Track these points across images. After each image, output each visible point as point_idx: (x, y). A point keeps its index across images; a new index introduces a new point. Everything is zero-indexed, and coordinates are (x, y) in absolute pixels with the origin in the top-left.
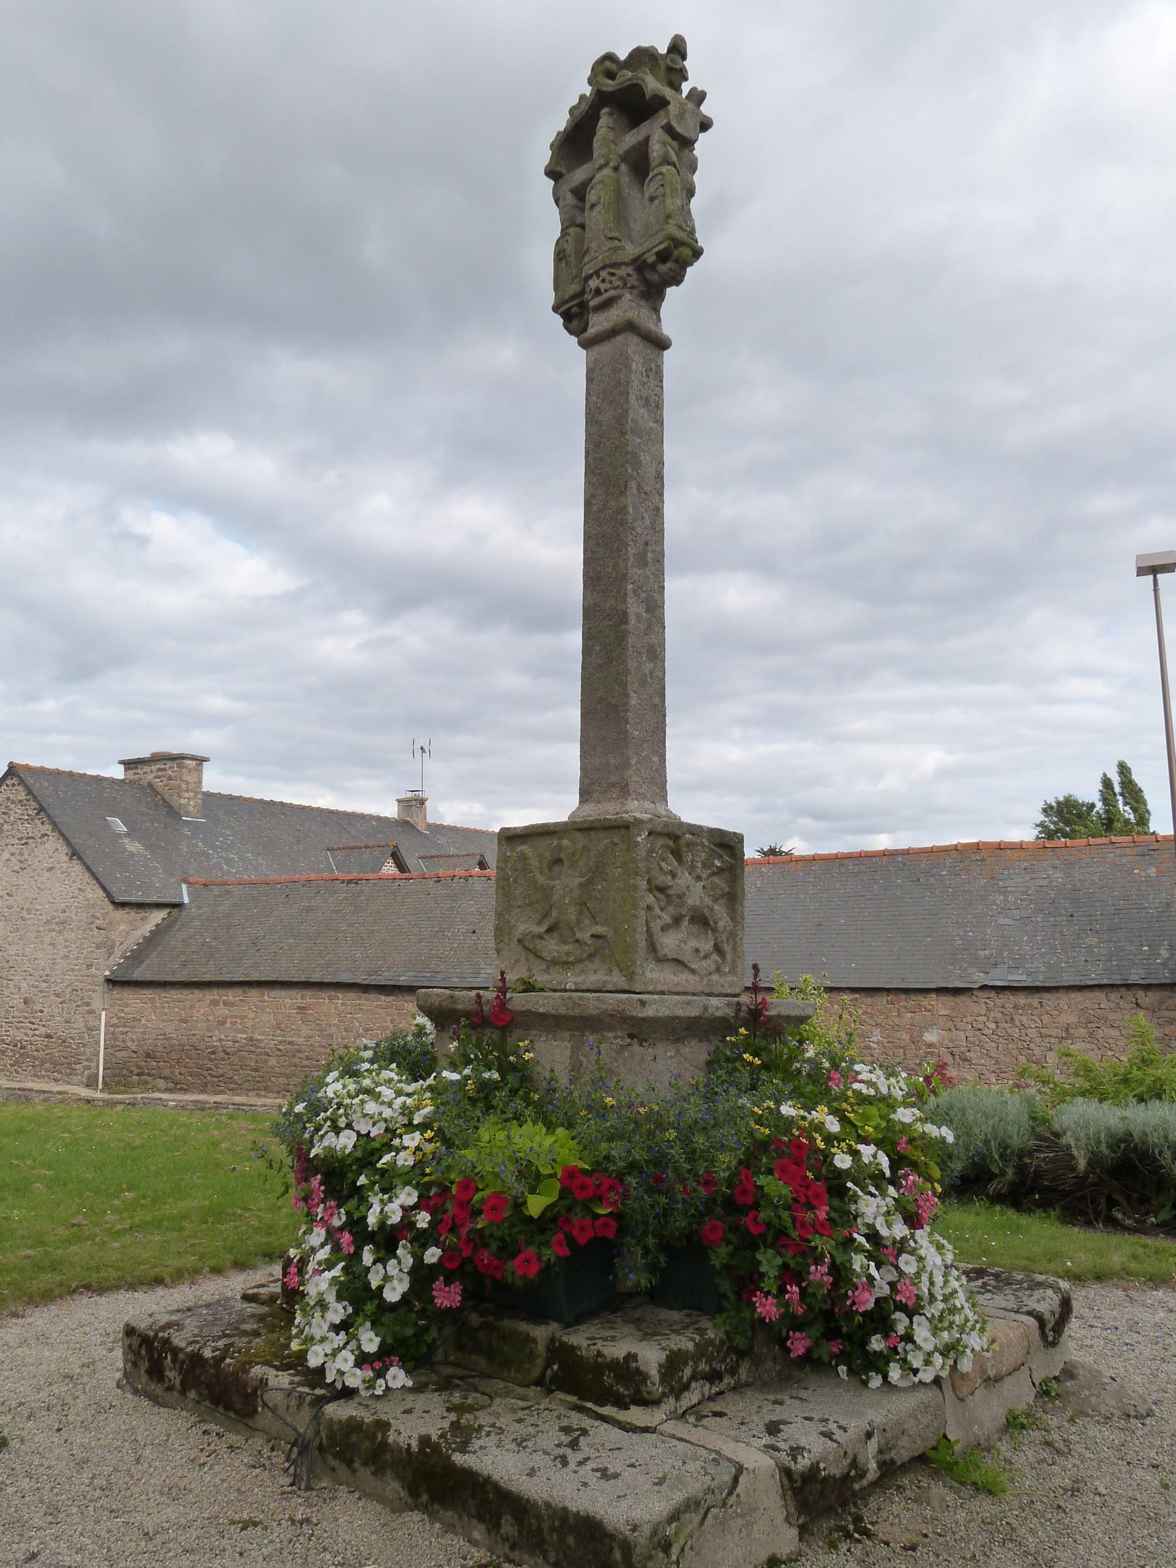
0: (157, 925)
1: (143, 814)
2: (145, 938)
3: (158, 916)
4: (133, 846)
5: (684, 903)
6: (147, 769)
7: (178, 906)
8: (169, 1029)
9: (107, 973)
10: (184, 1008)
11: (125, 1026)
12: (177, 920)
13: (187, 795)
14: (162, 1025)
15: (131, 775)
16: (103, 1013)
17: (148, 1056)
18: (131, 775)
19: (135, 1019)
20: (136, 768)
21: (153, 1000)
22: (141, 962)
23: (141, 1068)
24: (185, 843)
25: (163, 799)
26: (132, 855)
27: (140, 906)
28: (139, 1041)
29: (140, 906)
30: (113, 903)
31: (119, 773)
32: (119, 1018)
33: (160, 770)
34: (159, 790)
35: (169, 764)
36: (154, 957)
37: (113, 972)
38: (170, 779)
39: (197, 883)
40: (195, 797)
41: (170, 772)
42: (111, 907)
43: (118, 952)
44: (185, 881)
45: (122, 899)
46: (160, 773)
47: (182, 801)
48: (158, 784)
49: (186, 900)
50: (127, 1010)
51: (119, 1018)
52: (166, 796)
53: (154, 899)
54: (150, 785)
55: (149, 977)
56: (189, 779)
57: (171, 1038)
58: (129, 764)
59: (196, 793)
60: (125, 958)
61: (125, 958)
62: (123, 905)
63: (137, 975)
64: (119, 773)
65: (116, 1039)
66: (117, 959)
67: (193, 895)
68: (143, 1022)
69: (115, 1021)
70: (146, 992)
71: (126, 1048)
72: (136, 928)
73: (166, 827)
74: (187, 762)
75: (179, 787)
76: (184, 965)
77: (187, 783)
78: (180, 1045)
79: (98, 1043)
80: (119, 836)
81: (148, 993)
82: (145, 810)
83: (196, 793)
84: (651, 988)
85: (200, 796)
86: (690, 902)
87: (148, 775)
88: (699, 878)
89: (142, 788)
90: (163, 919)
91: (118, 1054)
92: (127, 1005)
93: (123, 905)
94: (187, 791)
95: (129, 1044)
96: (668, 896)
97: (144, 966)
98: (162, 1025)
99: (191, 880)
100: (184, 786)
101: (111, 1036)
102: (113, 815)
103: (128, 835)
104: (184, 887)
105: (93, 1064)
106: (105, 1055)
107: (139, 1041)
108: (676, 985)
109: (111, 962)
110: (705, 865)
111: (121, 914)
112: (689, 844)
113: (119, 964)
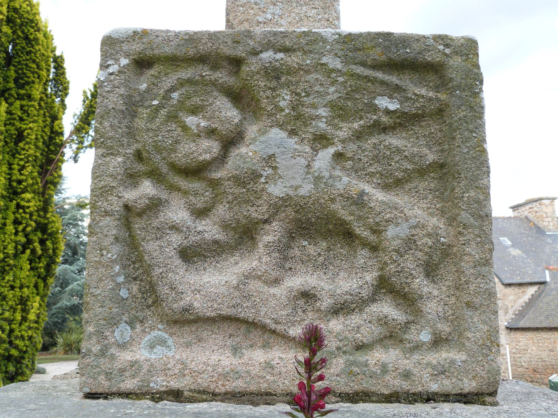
0: (532, 295)
1: (522, 234)
2: (526, 303)
3: (532, 290)
4: (515, 252)
5: (258, 195)
6: (523, 209)
7: (543, 283)
8: (544, 355)
9: (506, 324)
10: (550, 343)
11: (520, 353)
12: (543, 291)
13: (547, 220)
14: (539, 353)
15: (516, 214)
16: (507, 346)
17: (535, 371)
18: (516, 214)
19: (524, 350)
20: (518, 209)
21: (532, 339)
22: (524, 317)
23: (532, 378)
24: (548, 247)
25: (534, 224)
26: (514, 257)
27: (520, 285)
28: (528, 362)
29: (520, 285)
30: (503, 284)
31: (510, 213)
32: (516, 349)
33: (530, 208)
34: (532, 219)
35: (534, 204)
36: (530, 314)
37: (509, 323)
38: (536, 212)
39: (554, 269)
40: (553, 220)
41: (535, 209)
42: (503, 287)
43: (511, 312)
44: (547, 268)
45: (507, 282)
46: (531, 210)
47: (545, 224)
48: (531, 216)
49: (548, 279)
50: (520, 344)
51: (516, 349)
52: (536, 222)
53: (528, 280)
54: (526, 217)
55: (528, 325)
56: (547, 211)
57: (545, 361)
58: (515, 208)
59: (553, 218)
60: (516, 315)
61: (516, 315)
62: (510, 285)
63: (521, 324)
64: (510, 213)
65: (516, 361)
66: (510, 315)
67: (552, 277)
68: (529, 351)
69: (514, 350)
70: (527, 334)
71: (522, 366)
72: (520, 298)
73: (536, 239)
74: (544, 201)
75: (542, 216)
76: (547, 317)
77: (546, 213)
78: (551, 365)
79: (507, 363)
80: (507, 247)
81: (529, 335)
82: (523, 231)
83: (553, 218)
84: (129, 385)
85: (556, 219)
86: (277, 190)
87: (525, 212)
88: (321, 140)
89: (521, 219)
90: (536, 291)
91: (518, 369)
92: (519, 341)
93: (510, 285)
94: (547, 217)
95: (523, 364)
96: (214, 184)
97: (525, 319)
98: (539, 353)
99: (551, 267)
100: (544, 215)
101: (514, 359)
102: (504, 235)
103: (513, 246)
104: (547, 272)
105: (506, 375)
106: (512, 370)
107: (528, 362)
108: (225, 376)
109: (507, 317)
110: (340, 112)
111: (509, 290)
112: (274, 73)
113: (512, 318)
